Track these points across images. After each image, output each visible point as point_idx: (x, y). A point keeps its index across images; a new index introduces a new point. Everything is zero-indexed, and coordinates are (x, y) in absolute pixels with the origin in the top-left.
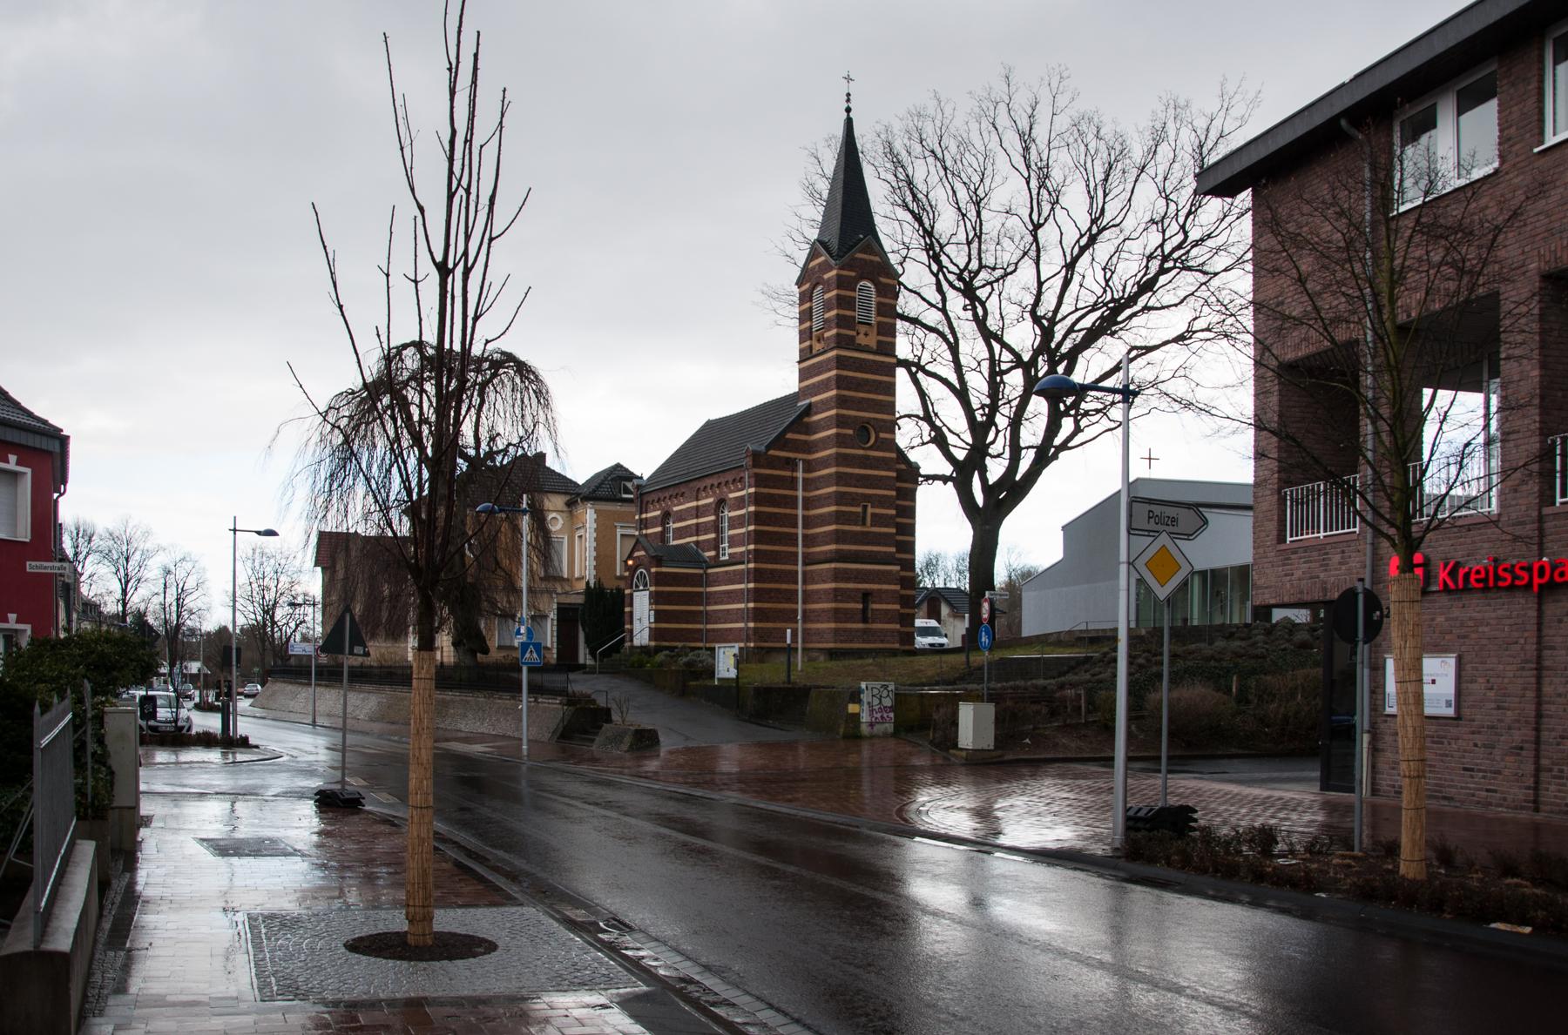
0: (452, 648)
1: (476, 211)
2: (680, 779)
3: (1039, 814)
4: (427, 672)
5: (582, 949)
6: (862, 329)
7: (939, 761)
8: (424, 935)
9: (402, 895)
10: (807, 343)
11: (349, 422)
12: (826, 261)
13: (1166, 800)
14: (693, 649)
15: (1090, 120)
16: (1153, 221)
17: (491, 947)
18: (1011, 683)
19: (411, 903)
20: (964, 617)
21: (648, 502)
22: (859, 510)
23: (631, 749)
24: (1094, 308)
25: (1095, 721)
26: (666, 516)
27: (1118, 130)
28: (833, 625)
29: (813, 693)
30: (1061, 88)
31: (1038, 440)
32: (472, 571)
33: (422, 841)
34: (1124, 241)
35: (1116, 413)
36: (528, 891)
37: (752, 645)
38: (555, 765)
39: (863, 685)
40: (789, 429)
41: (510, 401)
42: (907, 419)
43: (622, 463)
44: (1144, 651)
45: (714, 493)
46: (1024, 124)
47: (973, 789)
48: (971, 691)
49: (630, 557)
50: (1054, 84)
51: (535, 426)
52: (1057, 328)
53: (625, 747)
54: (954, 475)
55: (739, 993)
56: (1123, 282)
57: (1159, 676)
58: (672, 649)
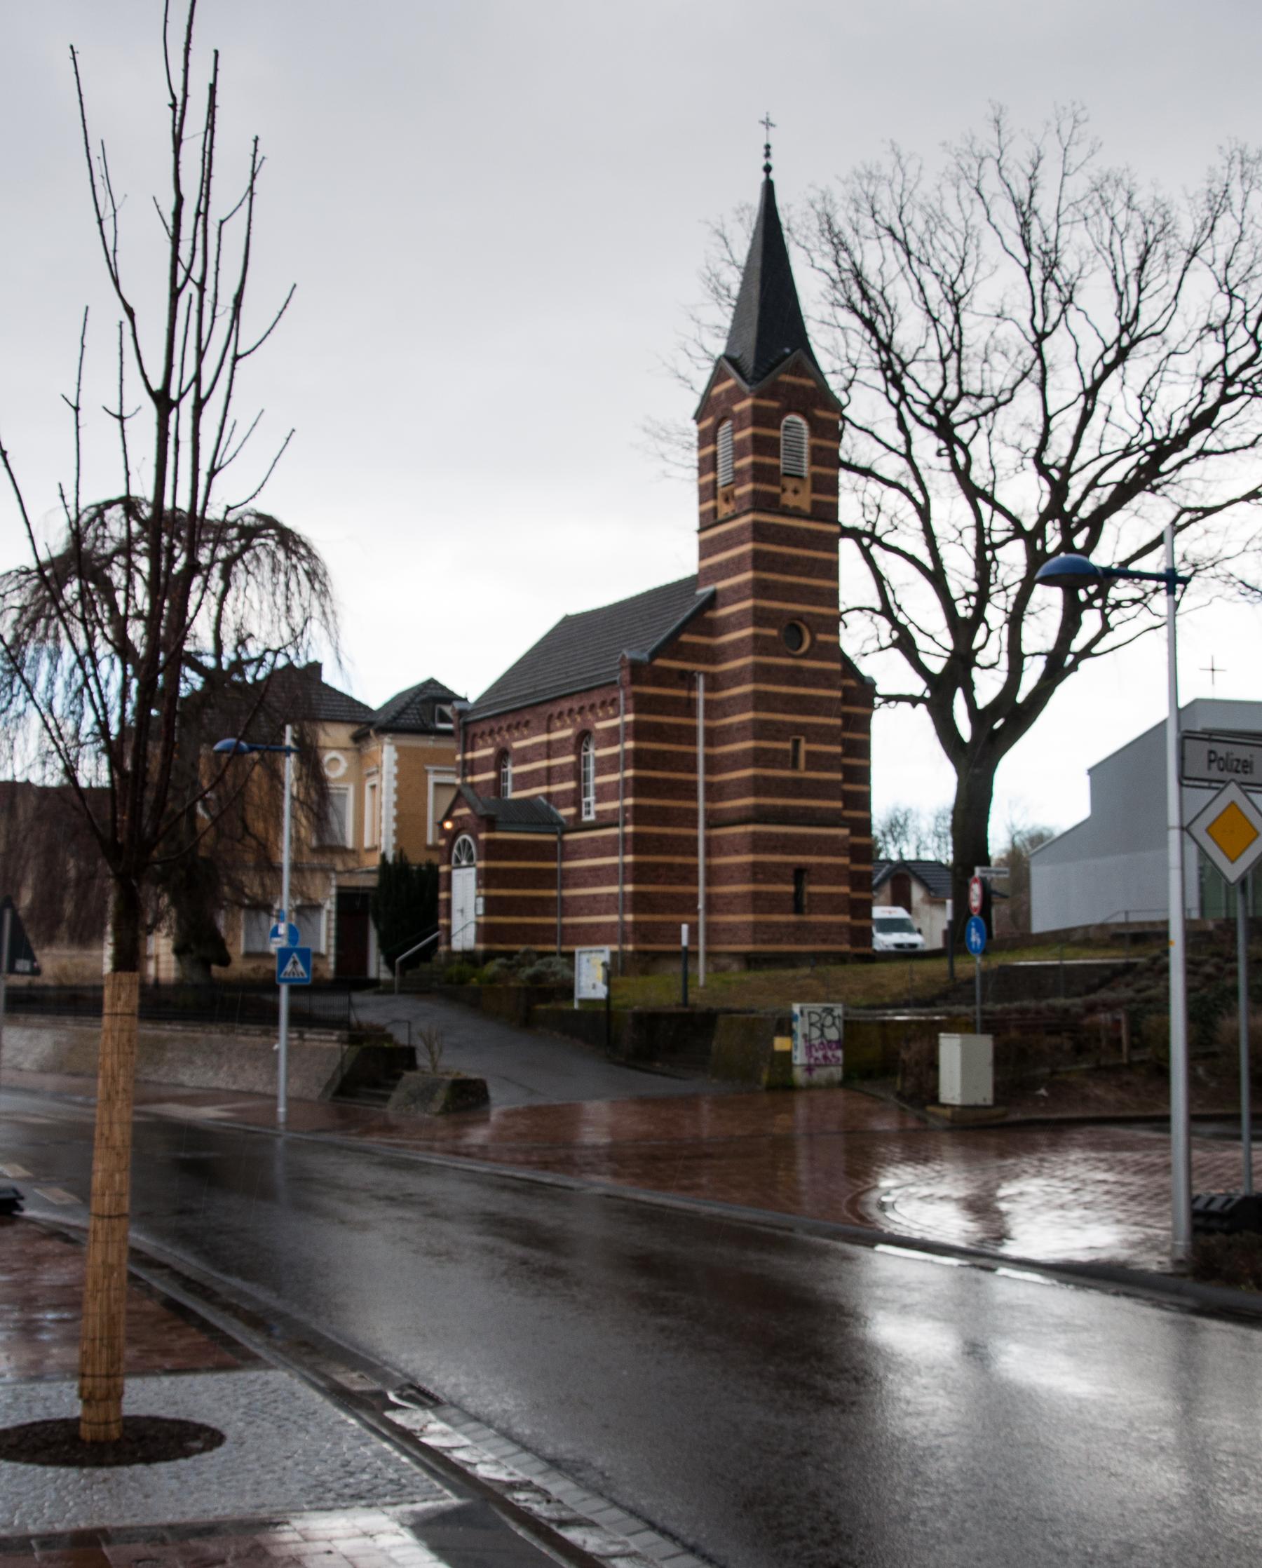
0: (173, 958)
1: (214, 317)
2: (520, 1157)
3: (1062, 1207)
4: (127, 1004)
5: (357, 1438)
6: (790, 484)
7: (911, 1124)
8: (107, 1423)
9: (72, 1356)
10: (710, 504)
11: (21, 615)
12: (736, 388)
13: (1251, 1184)
14: (542, 955)
15: (1118, 183)
16: (1210, 328)
17: (214, 1438)
18: (1016, 1004)
19: (88, 1371)
20: (944, 903)
21: (475, 736)
22: (788, 746)
23: (446, 1110)
24: (1127, 452)
25: (1142, 1062)
26: (503, 756)
27: (1159, 196)
28: (750, 918)
29: (722, 1021)
30: (1075, 137)
31: (1049, 644)
32: (208, 840)
33: (109, 1269)
34: (1168, 356)
35: (1160, 602)
36: (280, 1343)
37: (630, 947)
38: (325, 1137)
39: (796, 1008)
40: (682, 629)
41: (270, 588)
42: (856, 613)
43: (437, 678)
44: (1213, 955)
45: (574, 721)
46: (1022, 190)
47: (962, 1166)
48: (959, 1016)
49: (448, 816)
50: (1066, 132)
51: (305, 623)
52: (1072, 482)
53: (436, 1107)
54: (928, 694)
55: (600, 1504)
56: (1167, 415)
57: (1234, 992)
58: (509, 955)
